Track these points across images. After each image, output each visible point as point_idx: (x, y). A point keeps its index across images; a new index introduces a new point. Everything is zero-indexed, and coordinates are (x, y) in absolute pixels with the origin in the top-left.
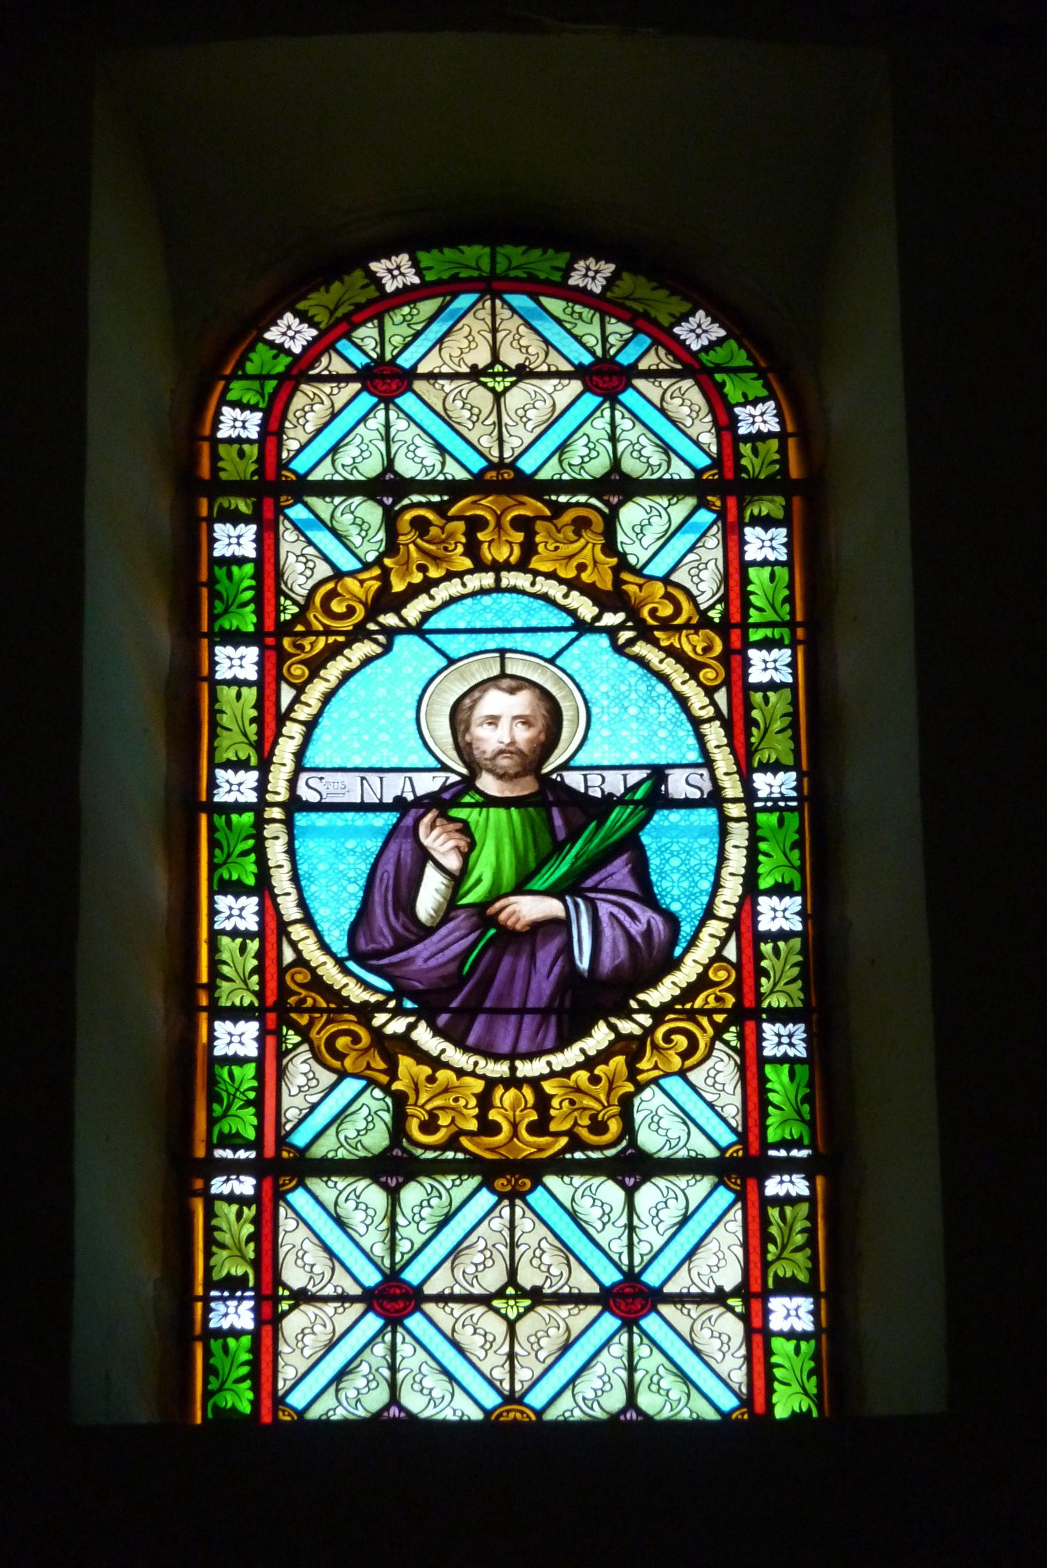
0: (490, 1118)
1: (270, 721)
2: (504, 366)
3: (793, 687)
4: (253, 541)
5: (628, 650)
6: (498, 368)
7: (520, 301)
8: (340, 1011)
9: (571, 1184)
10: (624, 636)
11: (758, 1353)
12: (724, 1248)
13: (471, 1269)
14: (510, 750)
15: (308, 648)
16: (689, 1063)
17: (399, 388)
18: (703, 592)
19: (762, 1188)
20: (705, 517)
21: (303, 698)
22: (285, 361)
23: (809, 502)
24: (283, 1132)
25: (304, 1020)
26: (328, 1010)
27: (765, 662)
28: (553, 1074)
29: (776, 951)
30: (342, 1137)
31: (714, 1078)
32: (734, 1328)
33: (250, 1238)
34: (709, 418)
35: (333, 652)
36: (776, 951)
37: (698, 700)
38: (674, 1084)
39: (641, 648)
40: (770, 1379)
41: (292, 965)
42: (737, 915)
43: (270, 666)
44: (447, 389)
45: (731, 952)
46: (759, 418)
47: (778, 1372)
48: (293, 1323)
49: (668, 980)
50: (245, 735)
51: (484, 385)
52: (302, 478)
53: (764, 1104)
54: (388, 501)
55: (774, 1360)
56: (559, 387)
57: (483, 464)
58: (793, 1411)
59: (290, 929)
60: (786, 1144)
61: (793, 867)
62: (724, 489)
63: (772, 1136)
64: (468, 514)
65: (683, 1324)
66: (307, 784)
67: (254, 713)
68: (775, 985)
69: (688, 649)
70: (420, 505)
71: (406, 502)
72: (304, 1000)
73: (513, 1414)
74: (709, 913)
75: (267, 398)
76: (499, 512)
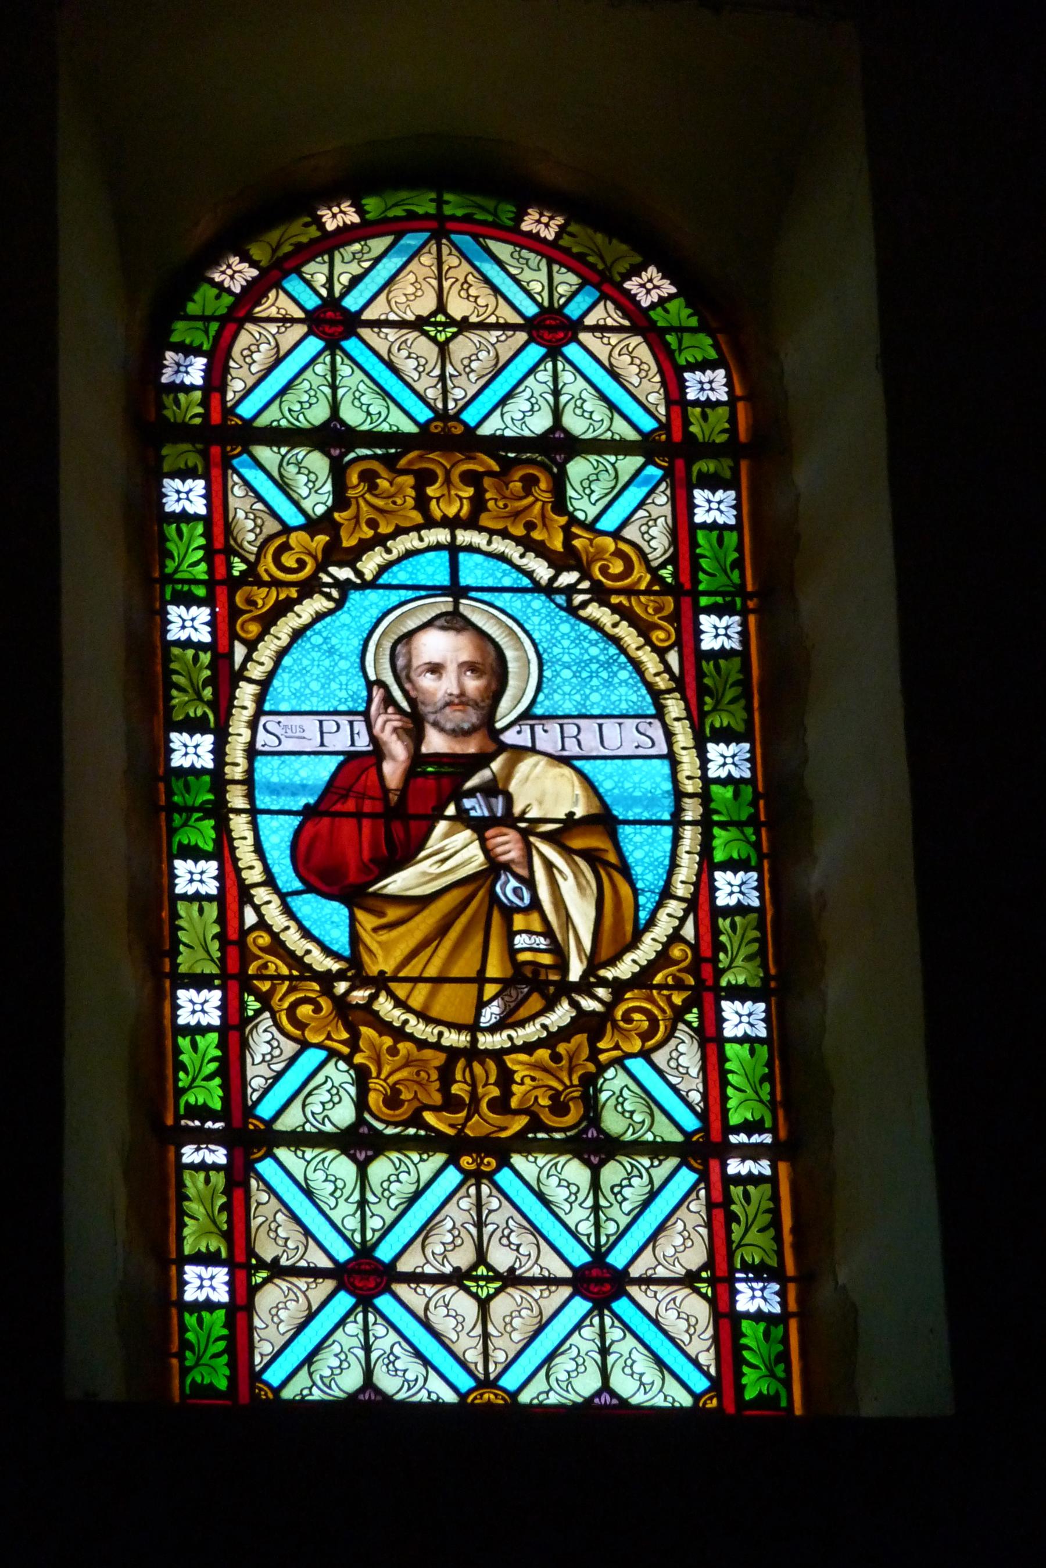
0: (453, 1092)
1: (226, 677)
2: (490, 1268)
3: (761, 910)
4: (211, 752)
5: (583, 613)
6: (482, 1270)
7: (464, 241)
8: (301, 978)
9: (542, 1269)
10: (578, 599)
11: (713, 1059)
12: (689, 1228)
13: (439, 1249)
14: (461, 700)
15: (260, 603)
16: (650, 1044)
17: (378, 1285)
18: (655, 549)
19: (724, 1166)
20: (653, 472)
21: (255, 656)
22: (227, 300)
23: (755, 451)
24: (250, 1103)
25: (265, 986)
26: (290, 978)
27: (716, 628)
28: (514, 1049)
29: (747, 1196)
30: (316, 1377)
31: (677, 1060)
32: (699, 1308)
33: (222, 1208)
34: (658, 378)
35: (284, 608)
36: (747, 1196)
37: (651, 662)
38: (637, 1065)
39: (593, 611)
40: (724, 1083)
41: (253, 928)
42: (695, 895)
43: (223, 627)
44: (391, 338)
45: (689, 931)
46: (709, 385)
47: (704, 563)
48: (268, 1298)
49: (628, 957)
50: (214, 1222)
51: (467, 1290)
52: (248, 423)
53: (739, 1361)
54: (336, 452)
55: (728, 1066)
56: (503, 338)
57: (430, 415)
58: (760, 1393)
59: (253, 892)
60: (748, 1127)
61: (761, 1101)
62: (675, 452)
63: (734, 1119)
64: (416, 467)
65: (650, 1305)
66: (264, 726)
67: (216, 929)
68: (732, 961)
69: (638, 610)
70: (366, 457)
71: (352, 455)
72: (265, 966)
73: (488, 1396)
74: (666, 894)
75: (211, 338)
76: (448, 467)
